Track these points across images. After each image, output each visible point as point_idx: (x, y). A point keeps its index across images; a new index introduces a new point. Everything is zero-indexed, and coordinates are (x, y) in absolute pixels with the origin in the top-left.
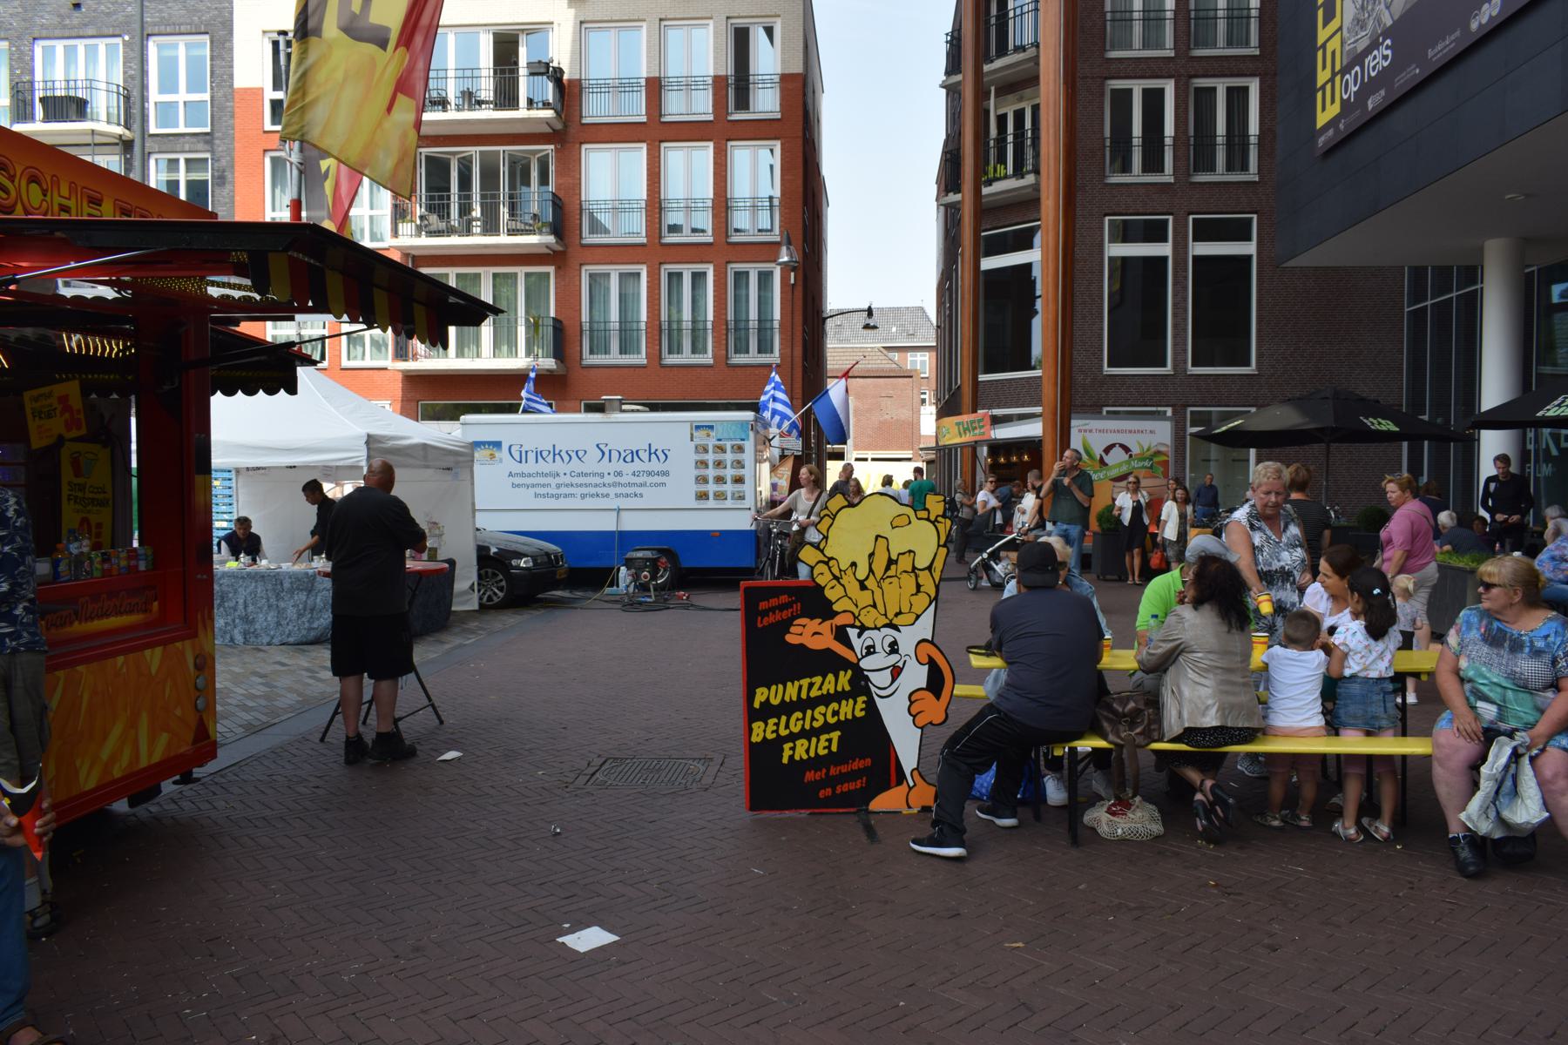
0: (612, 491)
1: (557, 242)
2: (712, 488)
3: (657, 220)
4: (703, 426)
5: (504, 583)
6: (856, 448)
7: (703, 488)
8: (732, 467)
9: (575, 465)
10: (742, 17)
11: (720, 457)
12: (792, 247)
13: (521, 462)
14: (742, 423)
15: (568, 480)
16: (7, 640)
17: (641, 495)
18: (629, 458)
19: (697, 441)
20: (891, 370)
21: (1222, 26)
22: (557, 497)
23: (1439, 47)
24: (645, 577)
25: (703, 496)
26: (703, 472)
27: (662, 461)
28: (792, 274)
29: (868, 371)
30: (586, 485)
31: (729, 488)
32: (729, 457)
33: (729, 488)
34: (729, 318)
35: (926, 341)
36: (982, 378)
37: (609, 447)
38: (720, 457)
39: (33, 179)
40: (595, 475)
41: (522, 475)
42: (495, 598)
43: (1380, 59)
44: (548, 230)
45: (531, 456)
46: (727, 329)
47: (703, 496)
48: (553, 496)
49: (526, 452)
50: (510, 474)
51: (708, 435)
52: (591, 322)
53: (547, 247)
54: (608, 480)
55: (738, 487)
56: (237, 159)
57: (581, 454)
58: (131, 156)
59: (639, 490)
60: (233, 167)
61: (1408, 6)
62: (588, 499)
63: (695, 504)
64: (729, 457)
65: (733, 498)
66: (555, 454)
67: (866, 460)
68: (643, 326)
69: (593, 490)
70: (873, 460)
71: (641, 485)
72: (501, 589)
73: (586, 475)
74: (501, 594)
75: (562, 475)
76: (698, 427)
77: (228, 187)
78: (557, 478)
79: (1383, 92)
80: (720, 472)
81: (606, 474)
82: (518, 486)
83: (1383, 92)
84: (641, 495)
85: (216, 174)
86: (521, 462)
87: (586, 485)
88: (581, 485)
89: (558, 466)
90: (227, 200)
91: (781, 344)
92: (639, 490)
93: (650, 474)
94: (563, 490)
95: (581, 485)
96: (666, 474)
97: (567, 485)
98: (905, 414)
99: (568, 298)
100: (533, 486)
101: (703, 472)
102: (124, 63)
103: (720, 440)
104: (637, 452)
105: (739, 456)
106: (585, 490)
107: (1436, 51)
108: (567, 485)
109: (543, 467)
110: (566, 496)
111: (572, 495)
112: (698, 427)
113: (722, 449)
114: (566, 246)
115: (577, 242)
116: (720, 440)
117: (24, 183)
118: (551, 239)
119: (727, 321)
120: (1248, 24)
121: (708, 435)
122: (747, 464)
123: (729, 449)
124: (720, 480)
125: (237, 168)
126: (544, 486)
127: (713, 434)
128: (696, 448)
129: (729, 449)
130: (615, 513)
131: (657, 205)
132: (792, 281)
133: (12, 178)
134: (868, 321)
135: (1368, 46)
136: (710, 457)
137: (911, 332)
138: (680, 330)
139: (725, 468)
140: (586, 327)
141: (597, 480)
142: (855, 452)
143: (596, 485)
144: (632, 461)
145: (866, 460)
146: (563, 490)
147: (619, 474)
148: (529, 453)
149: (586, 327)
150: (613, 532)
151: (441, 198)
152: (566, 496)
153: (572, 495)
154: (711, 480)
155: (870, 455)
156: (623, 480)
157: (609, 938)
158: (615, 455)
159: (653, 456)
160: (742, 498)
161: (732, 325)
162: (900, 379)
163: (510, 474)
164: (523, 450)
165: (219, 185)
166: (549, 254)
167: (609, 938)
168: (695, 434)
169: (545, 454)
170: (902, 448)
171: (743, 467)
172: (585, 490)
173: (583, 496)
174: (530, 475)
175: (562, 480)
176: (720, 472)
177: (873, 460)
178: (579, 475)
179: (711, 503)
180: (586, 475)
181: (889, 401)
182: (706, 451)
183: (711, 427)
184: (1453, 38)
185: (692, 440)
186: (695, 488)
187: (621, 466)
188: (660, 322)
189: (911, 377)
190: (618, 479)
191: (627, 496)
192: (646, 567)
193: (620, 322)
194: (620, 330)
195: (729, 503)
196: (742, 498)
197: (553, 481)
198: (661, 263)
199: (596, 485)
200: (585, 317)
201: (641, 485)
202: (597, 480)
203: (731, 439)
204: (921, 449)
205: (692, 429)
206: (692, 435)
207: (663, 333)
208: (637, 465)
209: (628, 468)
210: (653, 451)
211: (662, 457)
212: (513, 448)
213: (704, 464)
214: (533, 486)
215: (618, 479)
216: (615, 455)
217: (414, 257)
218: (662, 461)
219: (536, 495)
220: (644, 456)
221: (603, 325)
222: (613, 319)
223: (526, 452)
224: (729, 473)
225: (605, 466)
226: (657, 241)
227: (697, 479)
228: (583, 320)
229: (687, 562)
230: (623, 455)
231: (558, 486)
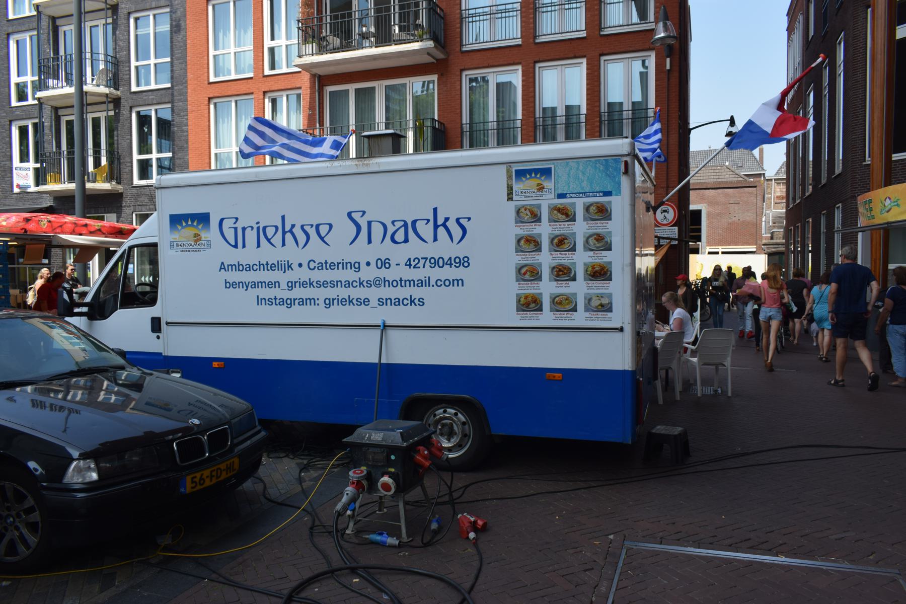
0: (373, 294)
1: (435, 46)
2: (547, 288)
3: (532, 20)
4: (530, 171)
5: (36, 517)
6: (709, 244)
7: (530, 289)
8: (587, 248)
9: (316, 250)
10: (626, 58)
11: (563, 228)
12: (669, 23)
13: (236, 246)
14: (606, 161)
15: (304, 274)
17: (422, 302)
18: (400, 236)
19: (519, 200)
20: (738, 182)
22: (289, 303)
24: (386, 487)
25: (530, 304)
26: (530, 258)
27: (456, 239)
28: (668, 60)
29: (720, 183)
30: (334, 284)
31: (580, 288)
32: (580, 228)
33: (580, 288)
34: (602, 110)
35: (751, 171)
36: (896, 157)
37: (367, 217)
38: (563, 228)
40: (345, 265)
41: (239, 267)
42: (21, 548)
44: (428, 36)
45: (251, 236)
46: (601, 121)
47: (530, 304)
48: (283, 302)
49: (244, 229)
50: (223, 267)
51: (541, 188)
52: (471, 123)
53: (429, 54)
54: (368, 274)
55: (598, 288)
56: (188, 9)
57: (324, 230)
58: (117, 17)
59: (417, 293)
60: (185, 16)
62: (335, 308)
63: (516, 320)
64: (580, 228)
65: (587, 309)
66: (285, 231)
67: (717, 253)
68: (519, 124)
69: (343, 293)
70: (723, 253)
71: (421, 283)
72: (33, 527)
73: (332, 266)
74: (33, 540)
75: (295, 266)
76: (520, 174)
77: (182, 33)
78: (289, 272)
80: (564, 259)
81: (363, 265)
82: (234, 285)
84: (422, 302)
85: (174, 23)
86: (236, 246)
87: (334, 284)
88: (324, 284)
89: (291, 253)
90: (182, 44)
92: (417, 293)
93: (435, 263)
94: (298, 292)
95: (324, 284)
96: (464, 262)
97: (303, 284)
98: (750, 216)
99: (450, 100)
100: (255, 285)
101: (530, 258)
103: (561, 196)
104: (414, 223)
105: (600, 227)
106: (331, 293)
108: (303, 284)
109: (268, 254)
110: (302, 302)
111: (312, 301)
112: (520, 174)
113: (567, 214)
114: (448, 54)
115: (458, 49)
116: (561, 196)
118: (430, 44)
119: (600, 113)
121: (541, 188)
122: (616, 241)
123: (580, 213)
124: (563, 273)
125: (188, 17)
126: (270, 285)
127: (548, 184)
128: (518, 212)
129: (580, 213)
130: (378, 332)
131: (532, 6)
132: (668, 67)
134: (731, 129)
136: (545, 230)
137: (740, 165)
138: (554, 125)
139: (573, 249)
140: (466, 128)
141: (349, 275)
142: (708, 247)
143: (348, 284)
144: (406, 241)
145: (717, 253)
146: (298, 292)
147: (384, 264)
148: (248, 231)
149: (466, 128)
150: (375, 364)
151: (343, 16)
152: (302, 302)
153: (312, 301)
154: (546, 273)
155: (720, 249)
156: (390, 274)
158: (377, 230)
159: (441, 230)
160: (606, 308)
161: (605, 117)
162: (746, 189)
163: (223, 267)
164: (240, 225)
165: (176, 33)
166: (433, 63)
168: (515, 187)
169: (270, 232)
170: (747, 243)
171: (609, 249)
172: (331, 293)
173: (329, 303)
174: (249, 268)
175: (296, 274)
176: (564, 259)
177: (723, 253)
178: (322, 266)
179: (547, 317)
180: (332, 266)
181: (736, 207)
182: (536, 218)
183: (546, 172)
185: (510, 198)
186: (513, 289)
187: (387, 250)
188: (535, 118)
189: (756, 187)
190: (383, 273)
191: (398, 302)
192: (389, 463)
193: (498, 121)
194: (498, 129)
195: (580, 318)
196: (606, 308)
197: (283, 278)
198: (535, 62)
199: (348, 284)
200: (465, 119)
201: (421, 283)
202: (349, 275)
203: (585, 194)
204: (763, 245)
205: (509, 177)
206: (510, 188)
208: (415, 248)
209: (399, 254)
210: (440, 221)
211: (457, 232)
212: (225, 222)
213: (531, 243)
214: (255, 285)
215: (383, 273)
216: (377, 230)
217: (320, 76)
218: (456, 239)
219: (260, 301)
220: (426, 230)
221: (482, 124)
222: (491, 119)
223: (244, 229)
224: (581, 259)
225: (362, 252)
226: (531, 40)
227: (519, 270)
228: (464, 122)
229: (501, 427)
230: (391, 229)
231: (291, 285)
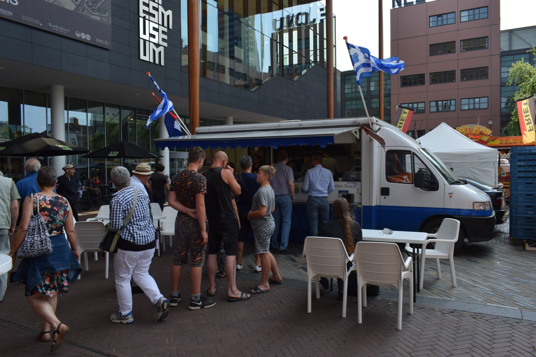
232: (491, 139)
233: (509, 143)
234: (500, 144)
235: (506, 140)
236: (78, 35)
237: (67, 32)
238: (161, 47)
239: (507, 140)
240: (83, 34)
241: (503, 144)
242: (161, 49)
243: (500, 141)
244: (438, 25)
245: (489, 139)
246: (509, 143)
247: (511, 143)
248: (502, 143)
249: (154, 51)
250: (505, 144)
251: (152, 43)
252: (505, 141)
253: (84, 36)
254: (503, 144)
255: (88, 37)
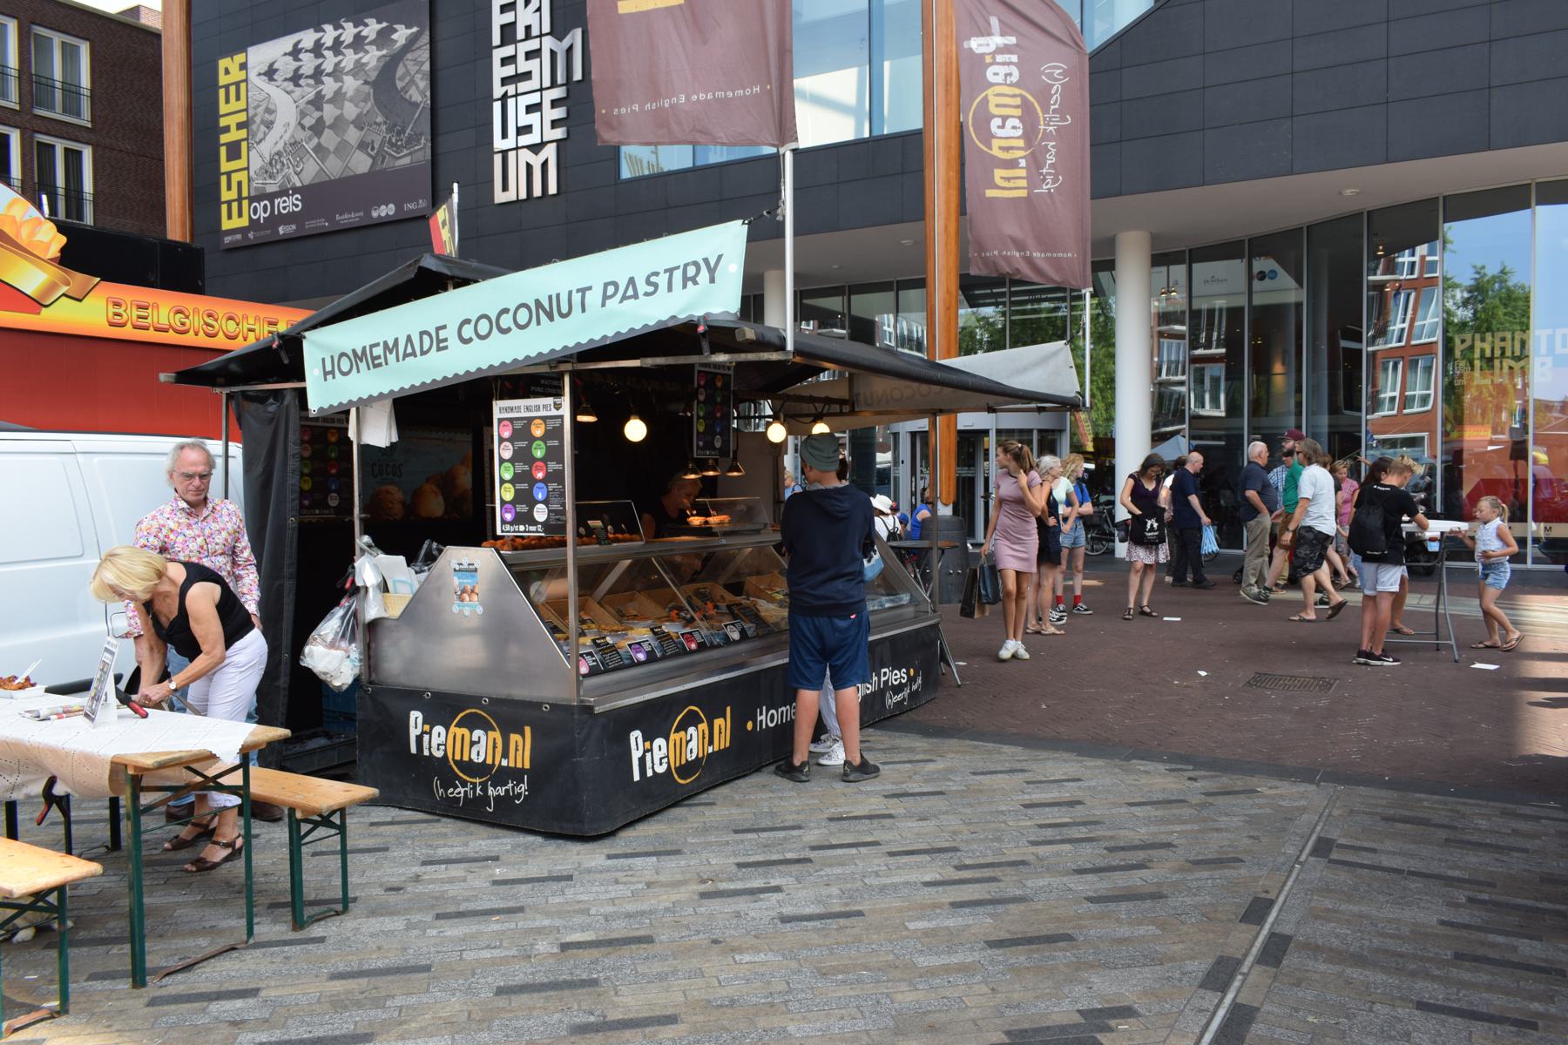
16: (416, 716)
21: (58, 95)
23: (346, 217)
39: (231, 318)
43: (291, 204)
61: (317, 181)
79: (294, 227)
83: (294, 227)
91: (268, 383)
102: (799, 295)
107: (343, 217)
117: (224, 321)
120: (53, 92)
133: (216, 320)
135: (276, 192)
157: (589, 522)
167: (589, 522)
184: (357, 215)
207: (1406, 401)
232: (64, 289)
233: (157, 330)
234: (112, 324)
235: (139, 307)
236: (375, 214)
237: (360, 217)
238: (549, 145)
239: (146, 308)
240: (383, 207)
241: (123, 325)
242: (550, 152)
243: (112, 310)
244: (544, 86)
245: (52, 287)
246: (157, 330)
247: (166, 331)
248: (142, 322)
249: (529, 167)
250: (135, 327)
251: (525, 150)
252: (135, 313)
253: (386, 211)
254: (123, 325)
255: (391, 209)
